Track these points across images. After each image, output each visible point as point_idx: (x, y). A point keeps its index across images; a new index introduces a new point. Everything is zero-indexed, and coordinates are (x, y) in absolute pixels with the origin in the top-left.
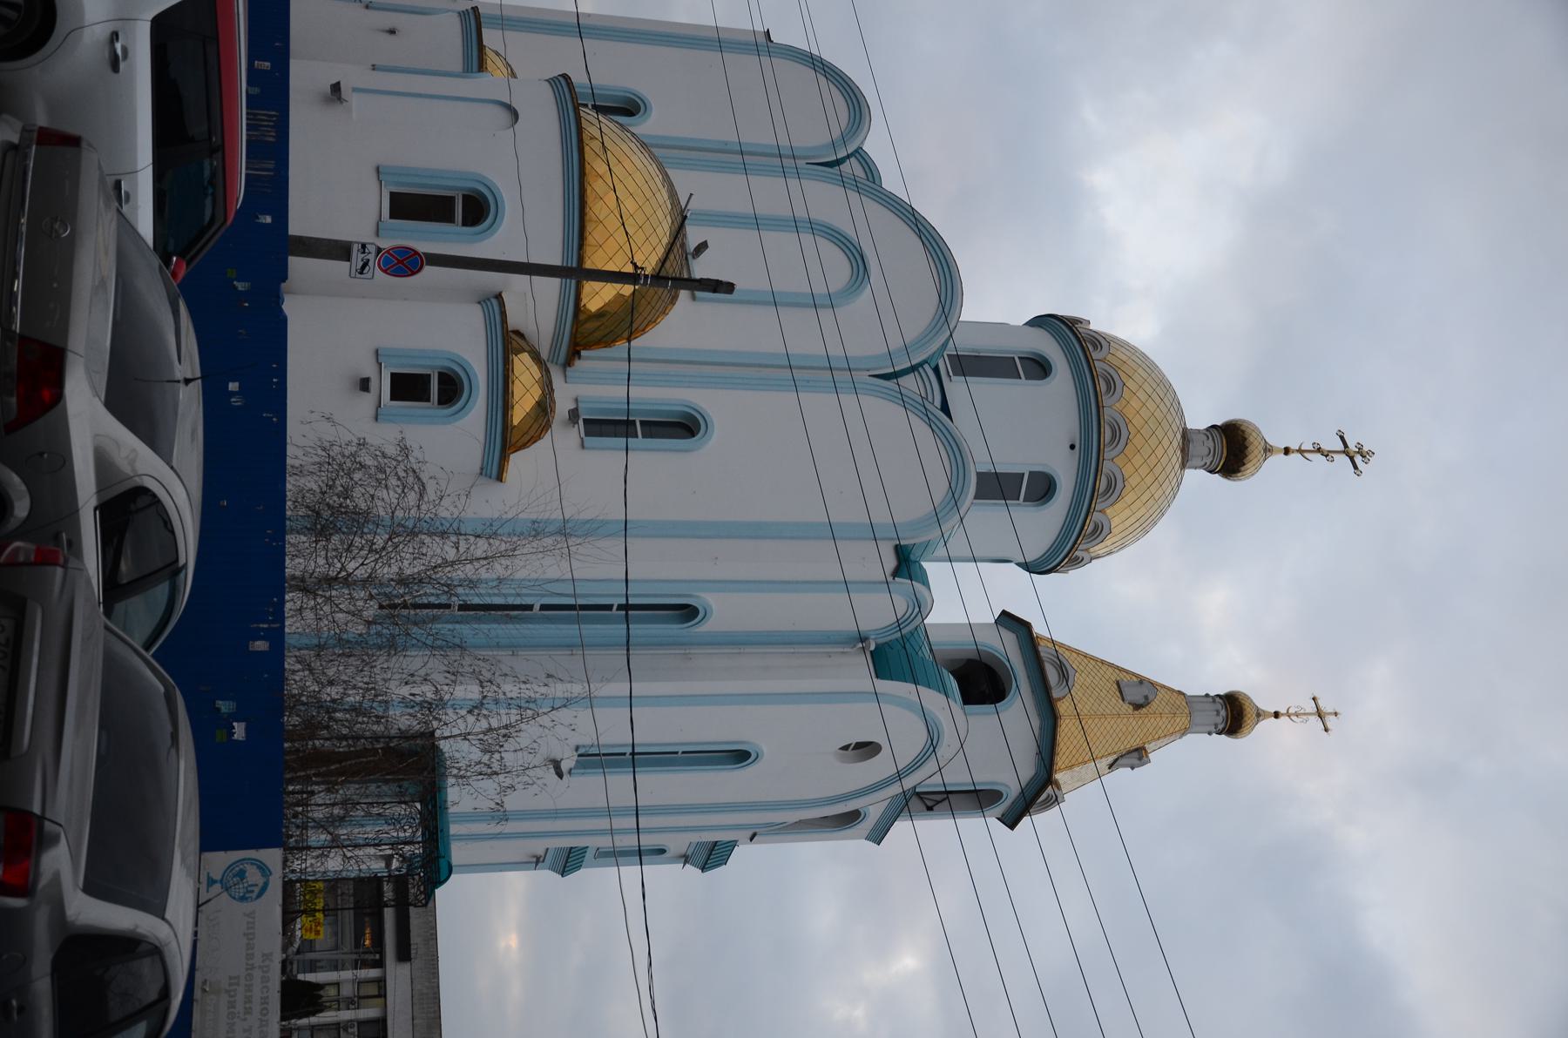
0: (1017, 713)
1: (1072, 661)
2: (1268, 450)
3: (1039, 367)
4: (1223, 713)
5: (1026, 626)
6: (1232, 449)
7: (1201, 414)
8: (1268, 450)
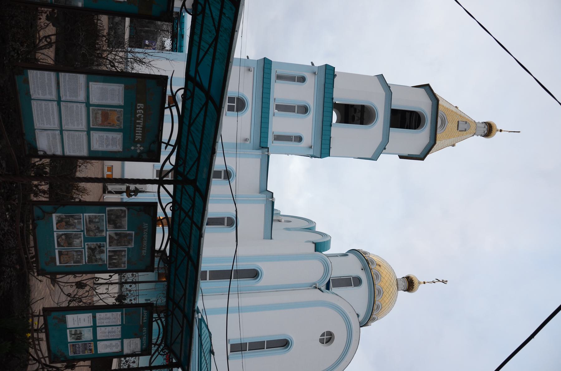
2: (420, 283)
3: (357, 281)
4: (486, 132)
5: (438, 100)
7: (401, 274)
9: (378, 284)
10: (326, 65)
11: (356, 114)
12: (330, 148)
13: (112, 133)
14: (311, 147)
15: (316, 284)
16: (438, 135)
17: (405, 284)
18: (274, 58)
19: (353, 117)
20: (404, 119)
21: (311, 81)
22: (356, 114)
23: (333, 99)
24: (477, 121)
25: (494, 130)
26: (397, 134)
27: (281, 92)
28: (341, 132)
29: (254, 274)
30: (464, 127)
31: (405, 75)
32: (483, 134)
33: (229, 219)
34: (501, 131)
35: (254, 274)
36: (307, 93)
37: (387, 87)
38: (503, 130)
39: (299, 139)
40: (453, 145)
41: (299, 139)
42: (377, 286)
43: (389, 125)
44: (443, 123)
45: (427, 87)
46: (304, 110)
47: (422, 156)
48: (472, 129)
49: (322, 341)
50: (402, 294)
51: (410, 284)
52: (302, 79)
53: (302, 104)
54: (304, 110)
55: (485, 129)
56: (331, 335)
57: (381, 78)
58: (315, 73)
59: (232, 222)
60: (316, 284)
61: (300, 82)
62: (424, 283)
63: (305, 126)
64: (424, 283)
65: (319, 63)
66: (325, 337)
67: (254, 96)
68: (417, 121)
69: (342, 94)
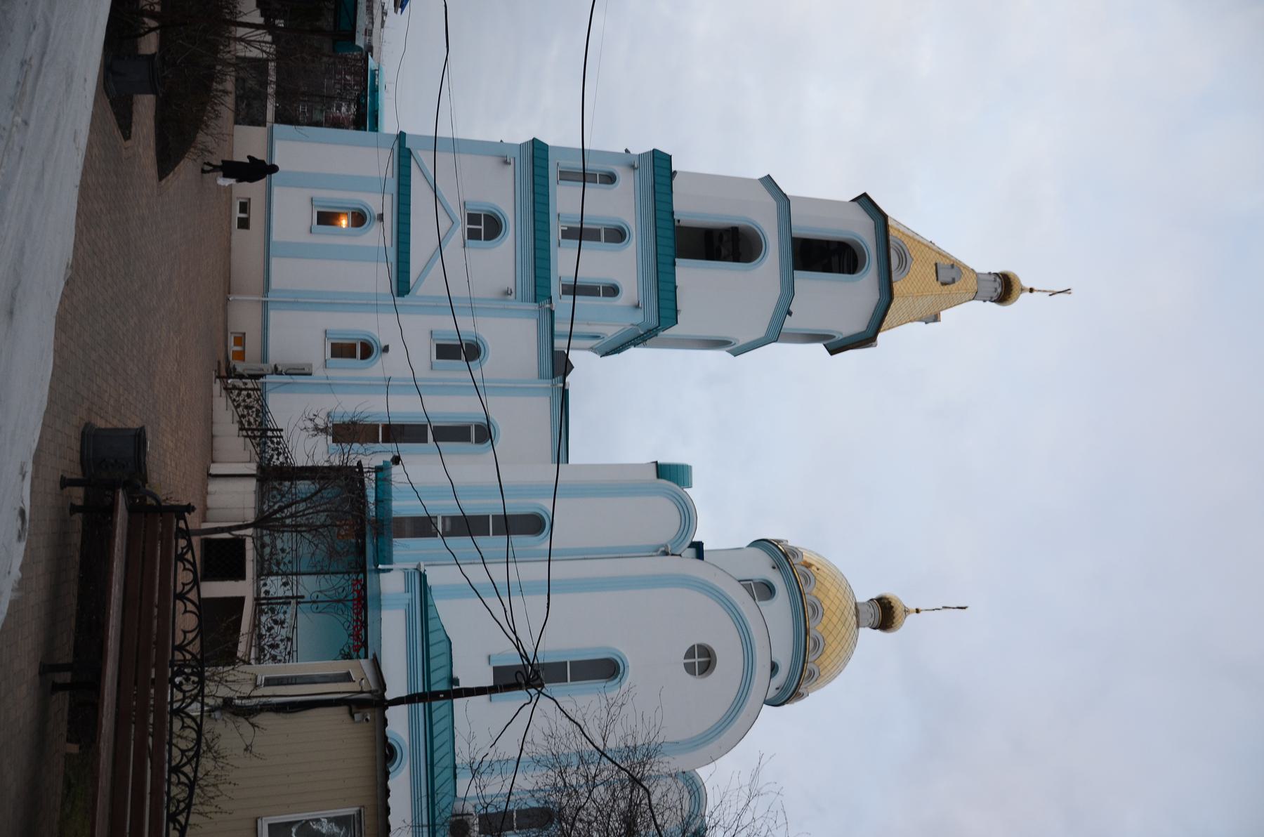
0: (863, 286)
1: (914, 253)
2: (907, 611)
4: (999, 290)
5: (885, 217)
6: (885, 614)
7: (865, 593)
8: (907, 611)
9: (811, 592)
10: (655, 152)
11: (728, 244)
12: (676, 311)
13: (118, 646)
14: (637, 306)
15: (666, 546)
16: (897, 287)
17: (875, 613)
18: (549, 140)
19: (724, 252)
20: (821, 255)
21: (627, 183)
22: (728, 244)
23: (673, 213)
24: (977, 271)
25: (1016, 289)
26: (811, 285)
27: (565, 201)
28: (693, 277)
29: (534, 524)
30: (950, 276)
31: (822, 182)
32: (995, 296)
33: (478, 427)
34: (1031, 290)
35: (534, 524)
36: (620, 204)
37: (783, 200)
38: (1035, 288)
39: (612, 291)
40: (936, 318)
41: (612, 291)
42: (808, 598)
43: (790, 267)
44: (903, 260)
45: (864, 201)
46: (617, 235)
47: (870, 334)
48: (972, 285)
49: (690, 669)
50: (869, 637)
51: (885, 614)
52: (610, 179)
53: (614, 223)
54: (617, 235)
55: (997, 285)
56: (709, 656)
57: (768, 182)
58: (633, 167)
59: (484, 433)
60: (666, 546)
61: (607, 183)
62: (918, 611)
63: (622, 266)
64: (918, 611)
65: (641, 147)
66: (697, 660)
67: (519, 273)
68: (850, 266)
69: (691, 207)
